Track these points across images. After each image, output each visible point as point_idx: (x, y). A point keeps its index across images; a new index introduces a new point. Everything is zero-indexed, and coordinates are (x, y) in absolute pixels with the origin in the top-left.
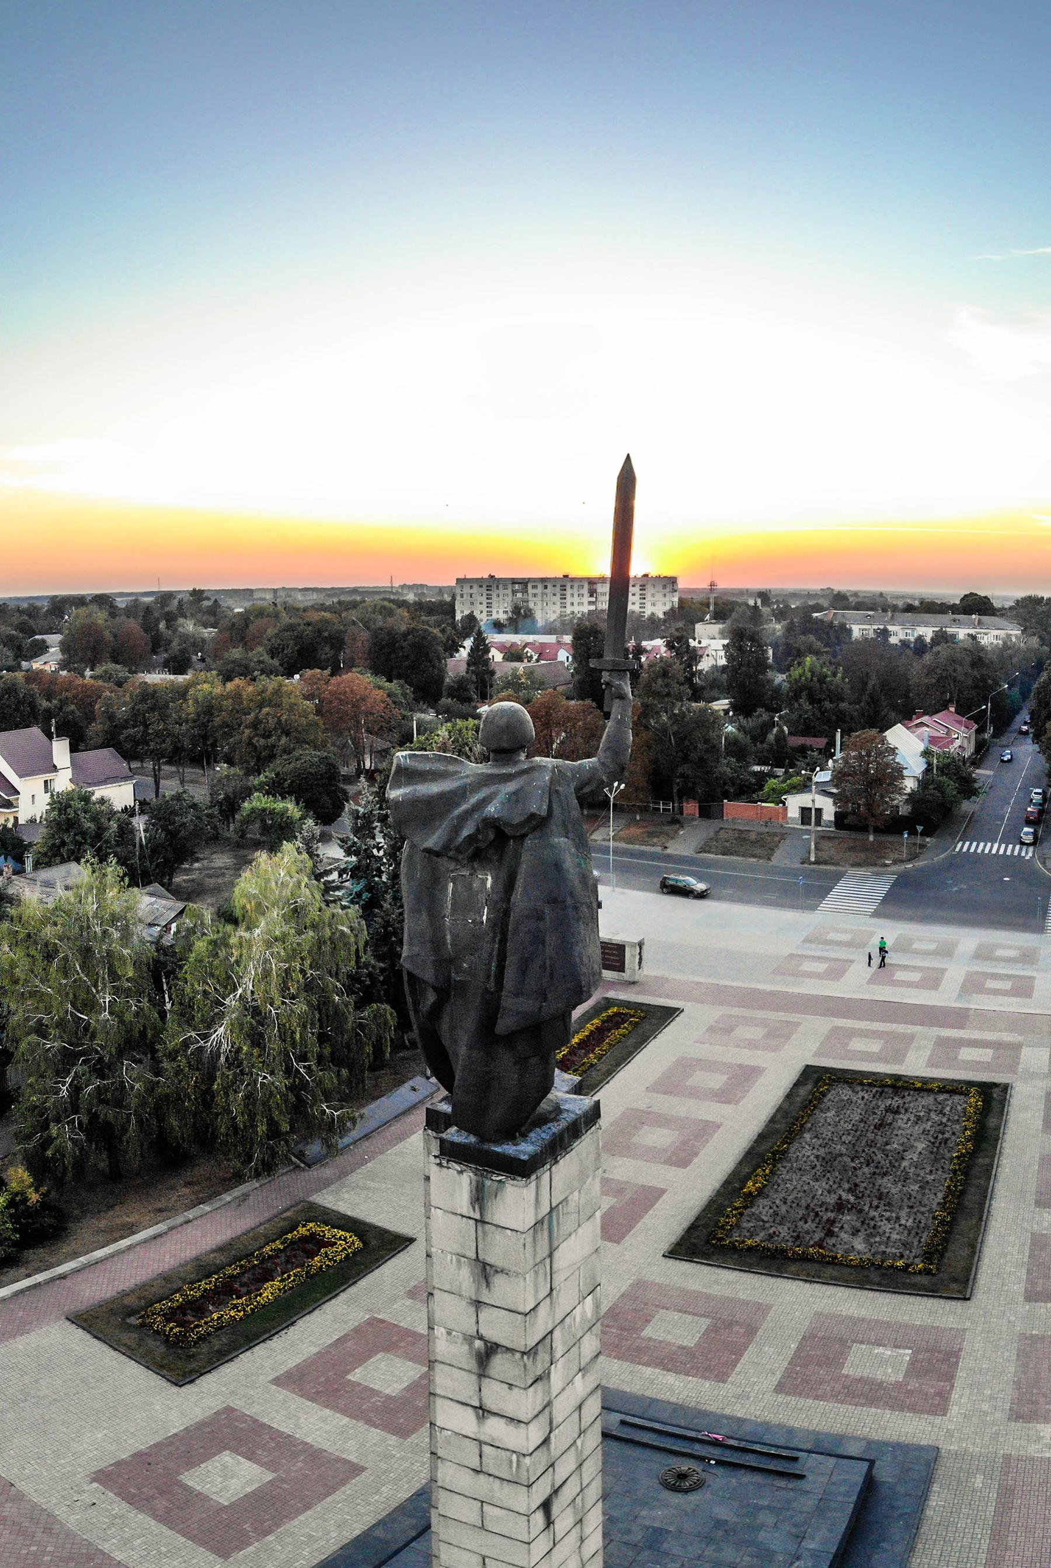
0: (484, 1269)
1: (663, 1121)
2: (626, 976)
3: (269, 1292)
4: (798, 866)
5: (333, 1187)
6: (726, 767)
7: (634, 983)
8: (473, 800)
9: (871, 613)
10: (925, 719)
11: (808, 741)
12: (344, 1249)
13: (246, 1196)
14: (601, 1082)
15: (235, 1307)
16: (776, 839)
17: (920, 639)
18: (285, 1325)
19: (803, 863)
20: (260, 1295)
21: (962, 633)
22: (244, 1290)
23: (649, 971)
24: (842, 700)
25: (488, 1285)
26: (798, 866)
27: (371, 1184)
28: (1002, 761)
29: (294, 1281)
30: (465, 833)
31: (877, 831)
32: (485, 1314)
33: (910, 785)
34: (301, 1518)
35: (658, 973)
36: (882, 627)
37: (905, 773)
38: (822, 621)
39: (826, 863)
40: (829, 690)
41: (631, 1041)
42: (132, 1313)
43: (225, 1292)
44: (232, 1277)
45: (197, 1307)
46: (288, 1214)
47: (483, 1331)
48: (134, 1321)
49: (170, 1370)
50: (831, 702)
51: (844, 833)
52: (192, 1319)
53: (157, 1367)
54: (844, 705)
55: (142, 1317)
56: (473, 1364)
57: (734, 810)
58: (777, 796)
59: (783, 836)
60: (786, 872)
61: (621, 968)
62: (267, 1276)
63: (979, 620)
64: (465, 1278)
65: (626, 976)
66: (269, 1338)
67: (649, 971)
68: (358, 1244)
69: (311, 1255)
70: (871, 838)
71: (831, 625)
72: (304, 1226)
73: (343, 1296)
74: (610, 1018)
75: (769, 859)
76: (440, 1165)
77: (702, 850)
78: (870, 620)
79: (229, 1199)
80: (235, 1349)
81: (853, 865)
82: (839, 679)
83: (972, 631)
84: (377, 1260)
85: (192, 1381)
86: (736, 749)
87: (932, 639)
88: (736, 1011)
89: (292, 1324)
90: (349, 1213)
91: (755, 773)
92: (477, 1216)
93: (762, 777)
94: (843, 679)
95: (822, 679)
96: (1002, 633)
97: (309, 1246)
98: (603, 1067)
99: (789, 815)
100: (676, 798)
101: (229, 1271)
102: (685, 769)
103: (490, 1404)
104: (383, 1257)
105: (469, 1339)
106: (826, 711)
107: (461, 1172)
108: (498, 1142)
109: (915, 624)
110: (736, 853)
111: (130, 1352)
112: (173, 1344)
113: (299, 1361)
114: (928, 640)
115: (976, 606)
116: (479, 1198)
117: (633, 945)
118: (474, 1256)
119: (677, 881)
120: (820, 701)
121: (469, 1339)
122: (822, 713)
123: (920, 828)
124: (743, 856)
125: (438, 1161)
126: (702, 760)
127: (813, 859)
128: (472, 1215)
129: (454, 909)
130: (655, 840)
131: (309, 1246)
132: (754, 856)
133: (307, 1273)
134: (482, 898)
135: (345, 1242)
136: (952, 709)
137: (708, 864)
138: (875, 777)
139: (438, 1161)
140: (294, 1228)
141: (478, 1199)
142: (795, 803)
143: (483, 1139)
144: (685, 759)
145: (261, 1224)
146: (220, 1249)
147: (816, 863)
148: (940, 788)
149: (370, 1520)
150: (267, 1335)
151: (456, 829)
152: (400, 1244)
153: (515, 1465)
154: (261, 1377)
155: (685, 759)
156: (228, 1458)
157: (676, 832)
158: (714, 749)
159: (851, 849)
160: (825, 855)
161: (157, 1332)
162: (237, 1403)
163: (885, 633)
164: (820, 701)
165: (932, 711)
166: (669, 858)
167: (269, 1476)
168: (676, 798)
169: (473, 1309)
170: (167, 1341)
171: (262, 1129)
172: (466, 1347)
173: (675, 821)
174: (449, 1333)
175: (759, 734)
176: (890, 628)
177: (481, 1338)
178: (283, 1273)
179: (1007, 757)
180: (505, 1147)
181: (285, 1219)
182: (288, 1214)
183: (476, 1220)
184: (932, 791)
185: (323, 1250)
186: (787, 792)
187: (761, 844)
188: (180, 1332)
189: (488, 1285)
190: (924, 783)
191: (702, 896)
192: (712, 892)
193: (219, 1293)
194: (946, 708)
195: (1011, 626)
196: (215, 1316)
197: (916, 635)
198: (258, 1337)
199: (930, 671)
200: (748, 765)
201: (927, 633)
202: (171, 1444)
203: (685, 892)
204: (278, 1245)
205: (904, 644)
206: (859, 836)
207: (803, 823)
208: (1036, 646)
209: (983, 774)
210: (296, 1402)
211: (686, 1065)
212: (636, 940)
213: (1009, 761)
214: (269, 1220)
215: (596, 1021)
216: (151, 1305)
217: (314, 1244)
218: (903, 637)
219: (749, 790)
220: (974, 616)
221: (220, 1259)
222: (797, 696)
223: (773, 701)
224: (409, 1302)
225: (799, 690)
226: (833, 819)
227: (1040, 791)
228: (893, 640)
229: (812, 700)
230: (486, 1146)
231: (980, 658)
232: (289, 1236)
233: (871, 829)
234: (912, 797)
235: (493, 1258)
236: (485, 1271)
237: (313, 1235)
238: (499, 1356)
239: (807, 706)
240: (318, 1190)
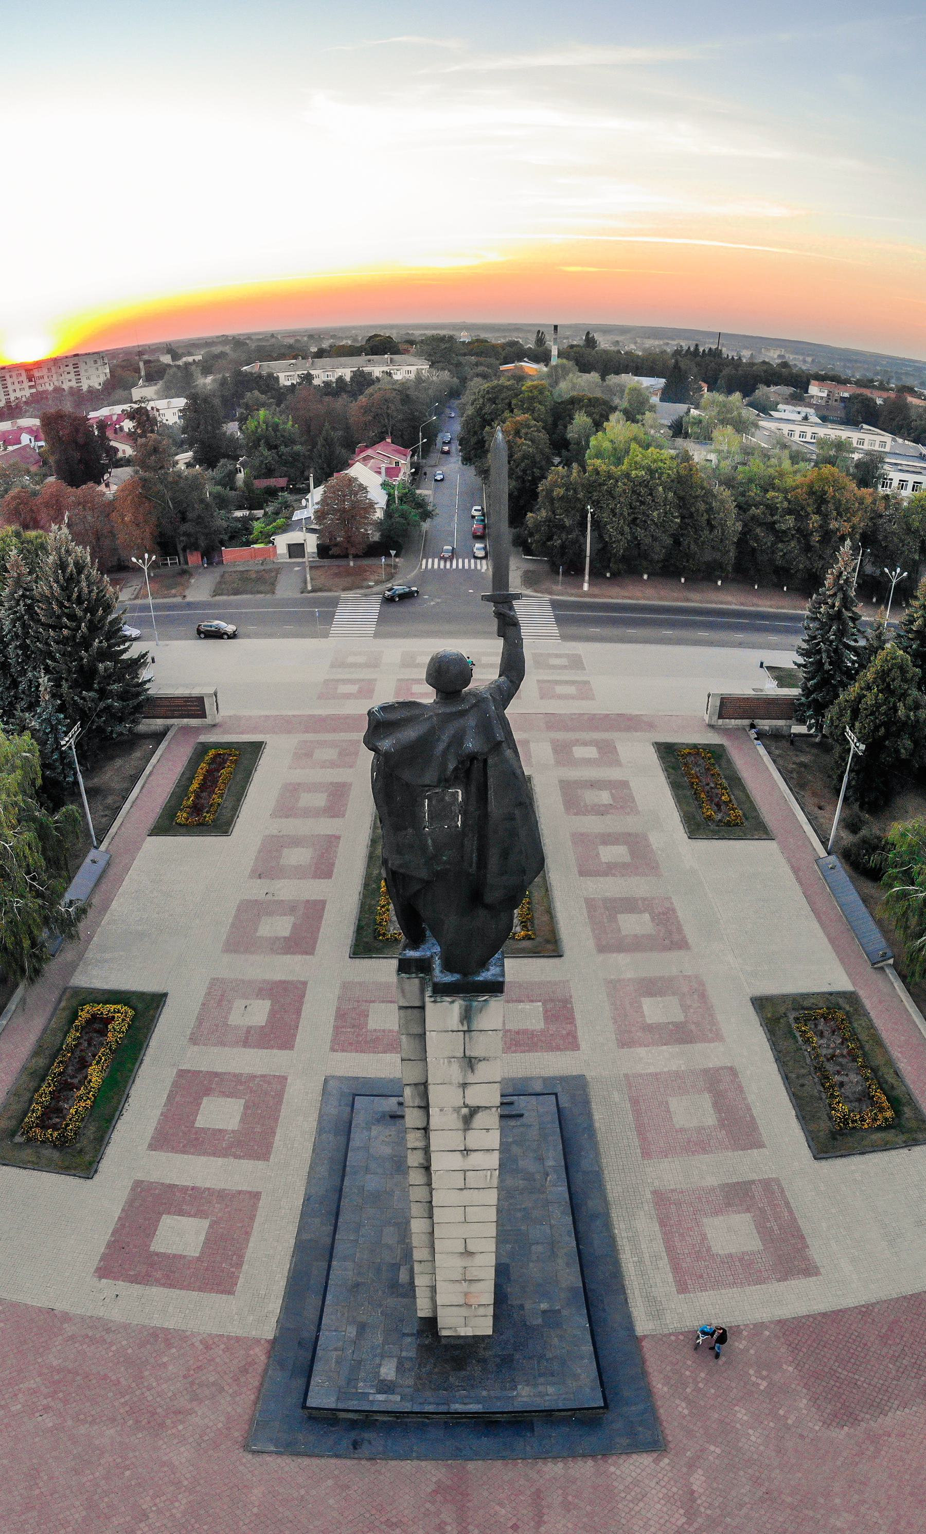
0: (470, 1061)
1: (296, 842)
2: (208, 721)
3: (95, 1075)
4: (299, 596)
5: (80, 969)
6: (220, 519)
7: (214, 725)
8: (445, 738)
9: (293, 361)
10: (369, 452)
11: (272, 482)
12: (123, 1020)
13: (23, 1001)
14: (233, 816)
15: (80, 1098)
16: (273, 574)
17: (340, 379)
18: (124, 1100)
19: (302, 593)
20: (90, 1081)
21: (377, 371)
22: (76, 1081)
23: (225, 712)
24: (294, 442)
25: (473, 1071)
26: (299, 596)
27: (107, 956)
28: (436, 480)
29: (106, 1060)
30: (451, 767)
31: (356, 557)
32: (470, 1091)
33: (379, 514)
34: (251, 1245)
35: (231, 713)
36: (305, 372)
37: (376, 506)
38: (251, 373)
39: (320, 590)
40: (282, 436)
41: (239, 777)
42: (13, 1134)
43: (64, 1088)
44: (60, 1074)
45: (53, 1111)
46: (63, 1004)
47: (468, 1102)
48: (19, 1139)
49: (75, 1168)
50: (286, 446)
51: (326, 562)
52: (58, 1120)
53: (65, 1169)
54: (298, 448)
55: (23, 1134)
56: (460, 1125)
57: (229, 554)
58: (267, 538)
59: (278, 571)
60: (294, 603)
61: (203, 716)
62: (84, 1064)
63: (391, 359)
64: (455, 1072)
65: (208, 721)
66: (121, 1115)
67: (225, 712)
68: (131, 1013)
69: (103, 1032)
70: (352, 564)
71: (260, 376)
72: (82, 1010)
73: (147, 1060)
74: (213, 760)
75: (274, 593)
76: (435, 1002)
77: (216, 593)
78: (294, 367)
79: (13, 1007)
80: (105, 1132)
81: (344, 590)
82: (289, 425)
83: (386, 369)
84: (152, 1021)
85: (96, 1171)
86: (222, 503)
87: (351, 378)
88: (310, 737)
89: (128, 1097)
90: (106, 987)
91: (237, 519)
92: (465, 1028)
93: (245, 521)
94: (293, 426)
95: (276, 428)
96: (413, 369)
97: (96, 1026)
98: (229, 804)
99: (278, 552)
100: (180, 552)
101: (57, 1069)
102: (184, 527)
103: (471, 1146)
104: (154, 1017)
105: (457, 1110)
106: (283, 454)
107: (453, 1002)
108: (478, 973)
109: (334, 368)
110: (245, 592)
111: (37, 1166)
112: (61, 1144)
113: (154, 1125)
114: (348, 378)
115: (380, 346)
116: (467, 1016)
117: (210, 695)
118: (462, 1055)
119: (211, 626)
120: (276, 447)
121: (457, 1110)
122: (280, 457)
123: (393, 552)
124: (252, 593)
125: (432, 999)
126: (199, 517)
127: (309, 588)
128: (461, 1028)
129: (431, 817)
130: (173, 591)
131: (96, 1026)
132: (261, 592)
133: (110, 1050)
134: (456, 809)
135: (122, 1015)
136: (389, 440)
137: (226, 605)
138: (346, 510)
139: (432, 999)
140: (75, 1016)
141: (466, 1017)
142: (282, 542)
143: (465, 975)
144: (184, 519)
145: (50, 1020)
146: (36, 1053)
147: (313, 591)
148: (403, 515)
149: (293, 1229)
150: (118, 1113)
151: (443, 766)
152: (161, 1000)
153: (489, 1177)
154: (139, 1148)
155: (184, 519)
156: (168, 1221)
157: (188, 581)
158: (207, 506)
159: (337, 575)
160: (318, 584)
161: (43, 1142)
162: (140, 1176)
163: (308, 377)
164: (276, 447)
165: (373, 443)
166: (190, 605)
167: (206, 1223)
168: (180, 552)
169: (461, 1089)
170: (55, 1146)
171: (26, 943)
172: (455, 1115)
173: (184, 572)
174: (441, 1110)
175: (228, 480)
176: (312, 372)
177: (466, 1106)
178: (94, 1056)
179: (439, 478)
180: (483, 974)
181: (64, 1009)
182: (63, 1004)
183: (464, 1031)
184: (397, 520)
185: (110, 1027)
186: (274, 533)
187: (263, 580)
188: (59, 1134)
189: (473, 1071)
190: (389, 513)
191: (233, 636)
192: (241, 631)
193: (60, 1091)
194: (383, 439)
195: (420, 362)
196: (72, 1111)
197: (336, 376)
198: (113, 1115)
199: (366, 410)
200: (229, 512)
201: (347, 373)
202: (123, 1226)
203: (218, 635)
204: (74, 1034)
205: (327, 384)
206: (341, 562)
207: (290, 557)
208: (448, 379)
209: (425, 492)
210: (162, 1156)
211: (293, 790)
212: (211, 691)
213: (442, 480)
214: (52, 1015)
215: (203, 765)
216: (22, 1120)
217: (99, 1024)
218: (326, 379)
219: (240, 535)
220: (386, 356)
221: (42, 1062)
222: (256, 445)
223: (230, 451)
224: (196, 1048)
225: (256, 441)
226: (316, 550)
227: (480, 508)
228: (316, 382)
229: (271, 447)
230: (470, 978)
231: (407, 396)
232: (77, 1023)
233: (351, 557)
234: (379, 524)
235: (475, 1051)
236: (470, 1063)
237: (94, 1016)
238: (480, 1114)
239: (266, 453)
240: (71, 974)
